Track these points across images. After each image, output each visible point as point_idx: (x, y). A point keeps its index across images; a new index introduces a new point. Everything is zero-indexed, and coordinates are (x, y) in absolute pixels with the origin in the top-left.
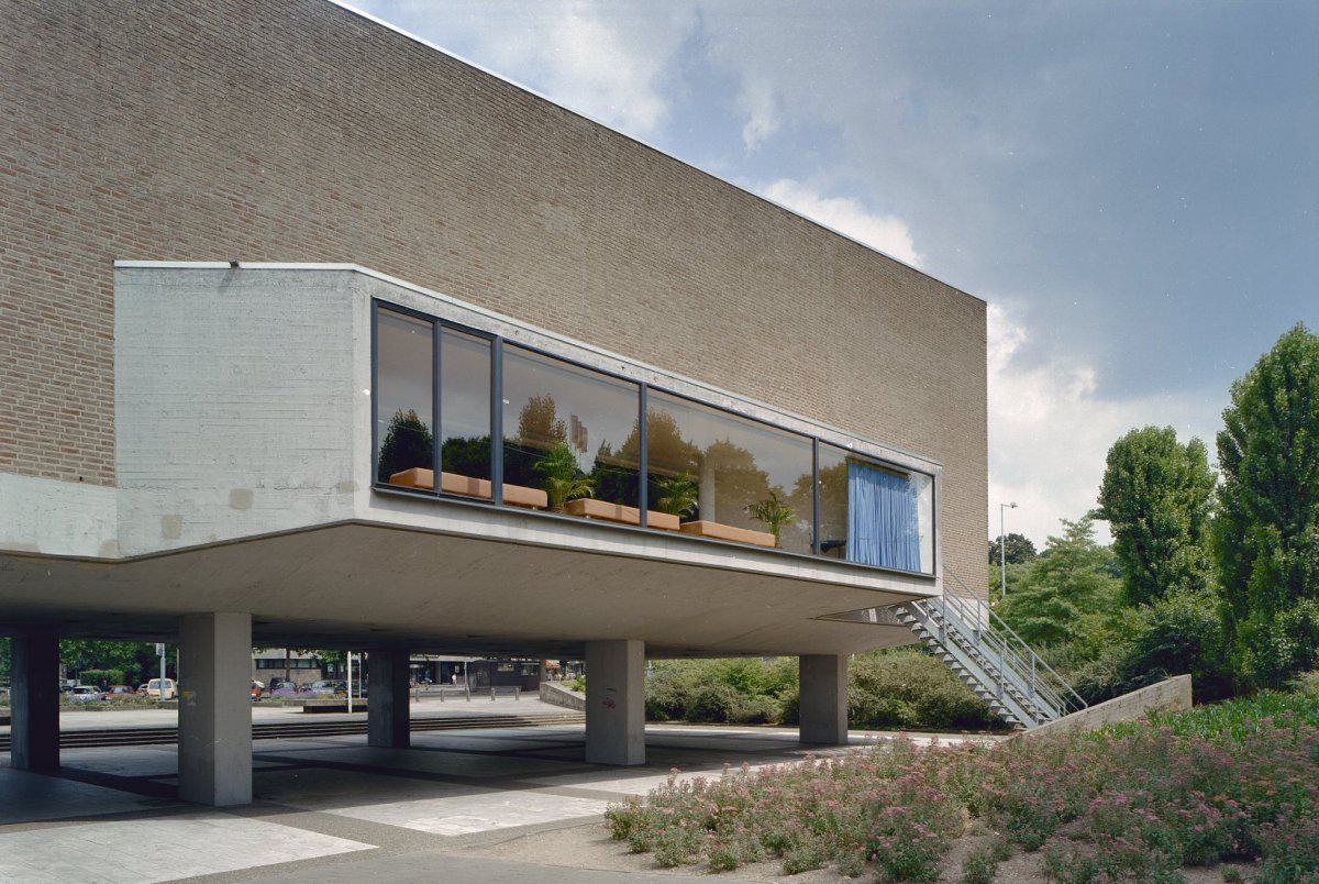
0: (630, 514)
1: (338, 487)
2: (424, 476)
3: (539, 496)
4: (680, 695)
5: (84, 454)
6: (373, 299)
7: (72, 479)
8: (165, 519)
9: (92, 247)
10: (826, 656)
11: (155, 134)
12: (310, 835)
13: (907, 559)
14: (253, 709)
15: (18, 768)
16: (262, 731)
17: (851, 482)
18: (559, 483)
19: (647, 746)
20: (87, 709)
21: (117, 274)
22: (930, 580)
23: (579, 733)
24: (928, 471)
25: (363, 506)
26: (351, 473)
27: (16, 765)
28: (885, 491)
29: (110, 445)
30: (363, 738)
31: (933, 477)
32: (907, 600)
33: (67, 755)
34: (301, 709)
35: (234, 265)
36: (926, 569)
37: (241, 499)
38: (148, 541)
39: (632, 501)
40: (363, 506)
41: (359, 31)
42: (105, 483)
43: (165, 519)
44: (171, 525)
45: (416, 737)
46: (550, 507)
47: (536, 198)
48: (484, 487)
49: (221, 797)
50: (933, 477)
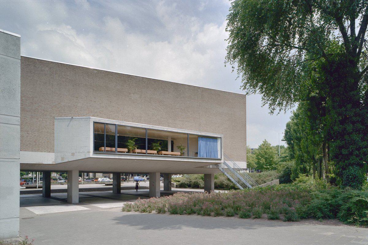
0: (144, 151)
1: (88, 152)
2: (103, 148)
3: (126, 150)
4: (191, 182)
5: (50, 148)
6: (94, 122)
7: (48, 152)
8: (62, 157)
9: (51, 116)
10: (209, 174)
11: (61, 97)
12: (83, 207)
13: (215, 156)
14: (67, 188)
15: (44, 197)
16: (81, 190)
17: (199, 142)
18: (130, 147)
19: (161, 193)
20: (61, 184)
21: (55, 120)
22: (220, 160)
23: (111, 193)
24: (220, 137)
25: (91, 154)
26: (90, 150)
27: (43, 196)
28: (208, 143)
29: (53, 146)
30: (112, 191)
31: (221, 138)
32: (217, 164)
33: (52, 194)
34: (105, 185)
35: (72, 118)
36: (219, 157)
37: (73, 154)
38: (59, 161)
39: (145, 149)
40: (91, 154)
41: (96, 72)
42: (53, 152)
43: (62, 157)
44: (63, 159)
45: (122, 191)
46: (129, 152)
47: (130, 94)
48: (114, 149)
49: (73, 202)
50: (221, 138)
